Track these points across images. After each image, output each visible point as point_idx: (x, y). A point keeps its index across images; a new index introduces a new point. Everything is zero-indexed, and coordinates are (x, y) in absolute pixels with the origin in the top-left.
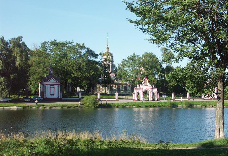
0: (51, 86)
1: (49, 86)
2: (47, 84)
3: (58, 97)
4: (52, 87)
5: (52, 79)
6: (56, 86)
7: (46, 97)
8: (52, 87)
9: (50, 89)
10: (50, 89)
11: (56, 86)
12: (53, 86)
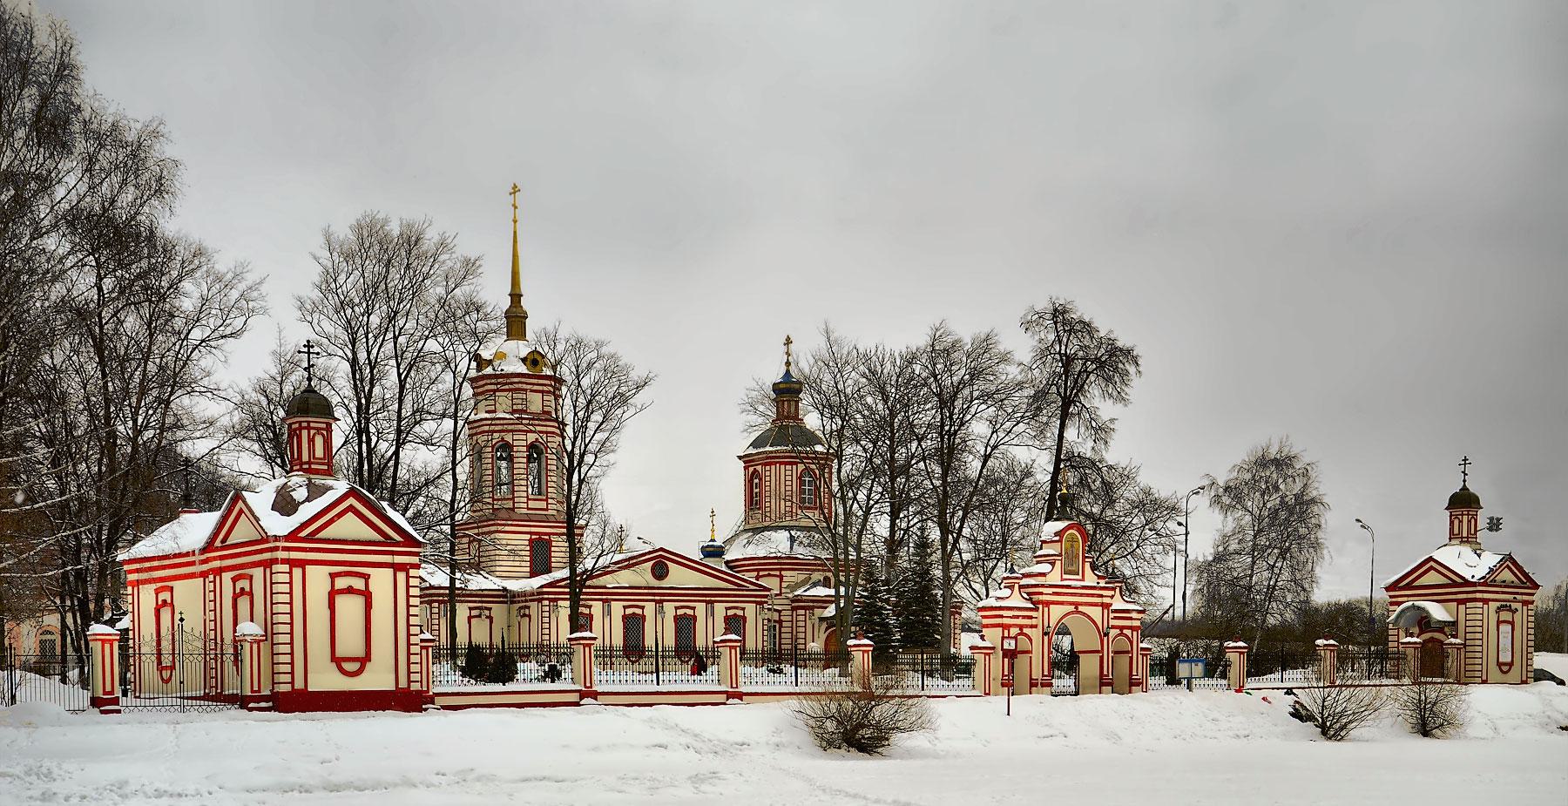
0: (341, 583)
4: (350, 590)
5: (351, 508)
7: (299, 685)
8: (350, 590)
12: (359, 584)
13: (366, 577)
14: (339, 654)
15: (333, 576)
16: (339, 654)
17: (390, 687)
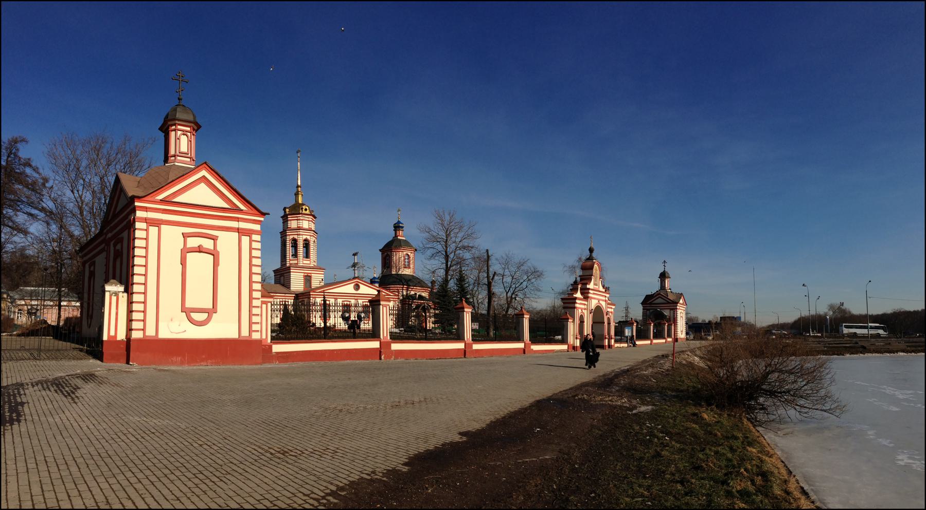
0: (193, 242)
1: (172, 237)
2: (157, 223)
3: (245, 333)
4: (200, 250)
6: (227, 242)
7: (151, 332)
8: (200, 250)
9: (183, 263)
10: (183, 263)
11: (227, 242)
12: (208, 244)
13: (214, 239)
14: (188, 305)
15: (185, 236)
16: (188, 305)
17: (236, 336)
